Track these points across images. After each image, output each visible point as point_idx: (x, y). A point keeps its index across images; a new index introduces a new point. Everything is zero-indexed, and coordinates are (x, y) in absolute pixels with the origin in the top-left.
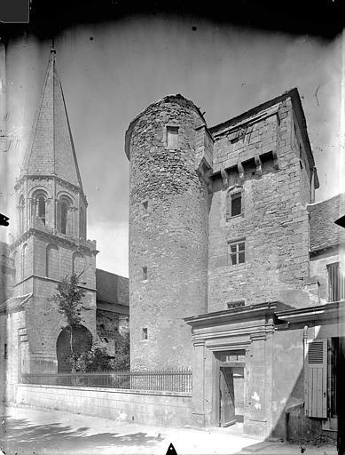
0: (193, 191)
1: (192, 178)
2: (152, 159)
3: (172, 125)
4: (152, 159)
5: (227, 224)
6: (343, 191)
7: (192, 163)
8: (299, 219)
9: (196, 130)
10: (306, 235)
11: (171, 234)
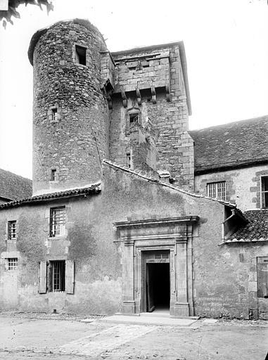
0: (98, 106)
1: (98, 95)
2: (61, 71)
3: (80, 45)
4: (61, 71)
5: (126, 138)
6: (266, 114)
7: (98, 82)
8: (187, 145)
9: (101, 53)
10: (192, 159)
11: (79, 142)
